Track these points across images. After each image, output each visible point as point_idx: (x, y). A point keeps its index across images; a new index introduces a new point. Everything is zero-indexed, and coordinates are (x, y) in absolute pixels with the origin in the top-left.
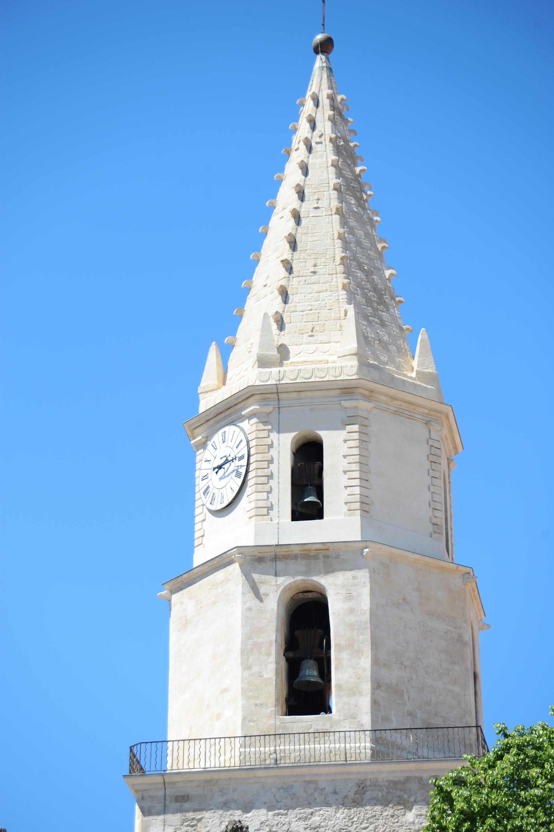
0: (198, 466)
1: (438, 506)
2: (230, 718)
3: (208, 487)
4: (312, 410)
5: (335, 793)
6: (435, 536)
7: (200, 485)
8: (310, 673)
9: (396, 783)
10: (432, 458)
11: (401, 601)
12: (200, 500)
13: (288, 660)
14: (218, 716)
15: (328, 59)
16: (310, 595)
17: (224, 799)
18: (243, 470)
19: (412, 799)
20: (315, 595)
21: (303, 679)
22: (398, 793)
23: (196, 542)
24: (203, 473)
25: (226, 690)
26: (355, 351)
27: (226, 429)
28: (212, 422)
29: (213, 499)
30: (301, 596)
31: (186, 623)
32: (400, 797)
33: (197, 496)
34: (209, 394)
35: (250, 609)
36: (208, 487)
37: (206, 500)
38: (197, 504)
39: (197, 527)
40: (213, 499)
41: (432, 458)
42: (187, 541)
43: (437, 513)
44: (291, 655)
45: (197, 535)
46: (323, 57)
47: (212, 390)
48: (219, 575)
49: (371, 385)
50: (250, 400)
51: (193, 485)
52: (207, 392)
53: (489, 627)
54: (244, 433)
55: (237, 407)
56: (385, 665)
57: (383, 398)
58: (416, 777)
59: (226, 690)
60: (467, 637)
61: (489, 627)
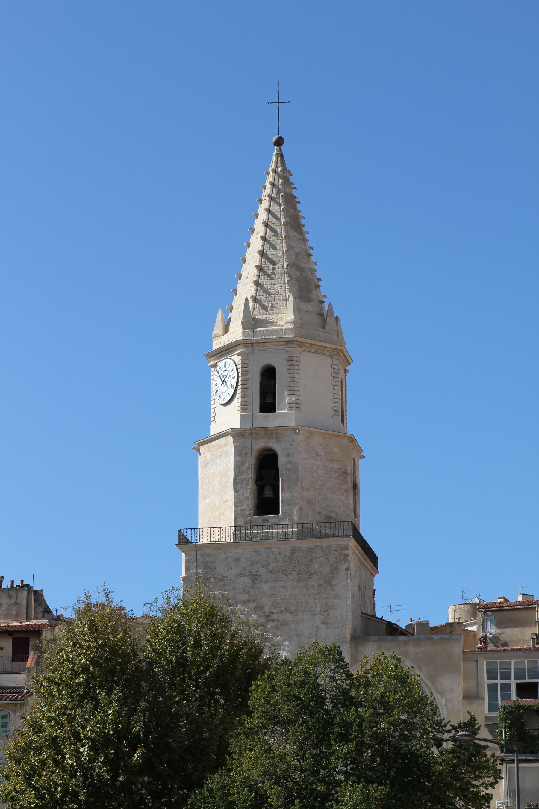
0: (212, 378)
1: (337, 401)
2: (227, 517)
3: (217, 391)
4: (270, 353)
5: (280, 553)
6: (335, 417)
7: (214, 389)
8: (268, 493)
9: (310, 549)
10: (334, 375)
11: (315, 455)
12: (214, 397)
13: (258, 485)
14: (223, 514)
15: (281, 149)
16: (269, 452)
17: (225, 556)
18: (235, 384)
19: (318, 556)
20: (272, 452)
21: (265, 496)
22: (311, 553)
23: (212, 419)
24: (214, 382)
25: (227, 501)
26: (293, 320)
27: (226, 360)
28: (219, 355)
29: (220, 398)
30: (264, 453)
31: (206, 464)
32: (311, 555)
33: (212, 394)
34: (217, 338)
35: (238, 461)
36: (217, 391)
37: (217, 398)
38: (212, 398)
39: (212, 411)
40: (220, 398)
41: (334, 375)
42: (206, 418)
43: (336, 404)
44: (259, 483)
45: (212, 415)
46: (278, 148)
47: (219, 336)
48: (222, 441)
49: (301, 340)
50: (238, 347)
51: (210, 388)
52: (217, 337)
53: (364, 457)
54: (236, 364)
55: (232, 349)
56: (306, 489)
57: (308, 345)
58: (319, 546)
59: (227, 501)
60: (350, 469)
61: (364, 457)
